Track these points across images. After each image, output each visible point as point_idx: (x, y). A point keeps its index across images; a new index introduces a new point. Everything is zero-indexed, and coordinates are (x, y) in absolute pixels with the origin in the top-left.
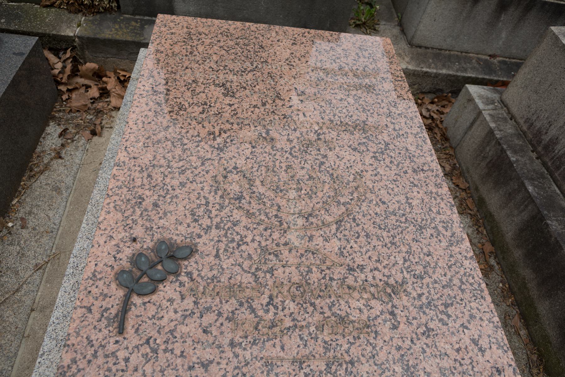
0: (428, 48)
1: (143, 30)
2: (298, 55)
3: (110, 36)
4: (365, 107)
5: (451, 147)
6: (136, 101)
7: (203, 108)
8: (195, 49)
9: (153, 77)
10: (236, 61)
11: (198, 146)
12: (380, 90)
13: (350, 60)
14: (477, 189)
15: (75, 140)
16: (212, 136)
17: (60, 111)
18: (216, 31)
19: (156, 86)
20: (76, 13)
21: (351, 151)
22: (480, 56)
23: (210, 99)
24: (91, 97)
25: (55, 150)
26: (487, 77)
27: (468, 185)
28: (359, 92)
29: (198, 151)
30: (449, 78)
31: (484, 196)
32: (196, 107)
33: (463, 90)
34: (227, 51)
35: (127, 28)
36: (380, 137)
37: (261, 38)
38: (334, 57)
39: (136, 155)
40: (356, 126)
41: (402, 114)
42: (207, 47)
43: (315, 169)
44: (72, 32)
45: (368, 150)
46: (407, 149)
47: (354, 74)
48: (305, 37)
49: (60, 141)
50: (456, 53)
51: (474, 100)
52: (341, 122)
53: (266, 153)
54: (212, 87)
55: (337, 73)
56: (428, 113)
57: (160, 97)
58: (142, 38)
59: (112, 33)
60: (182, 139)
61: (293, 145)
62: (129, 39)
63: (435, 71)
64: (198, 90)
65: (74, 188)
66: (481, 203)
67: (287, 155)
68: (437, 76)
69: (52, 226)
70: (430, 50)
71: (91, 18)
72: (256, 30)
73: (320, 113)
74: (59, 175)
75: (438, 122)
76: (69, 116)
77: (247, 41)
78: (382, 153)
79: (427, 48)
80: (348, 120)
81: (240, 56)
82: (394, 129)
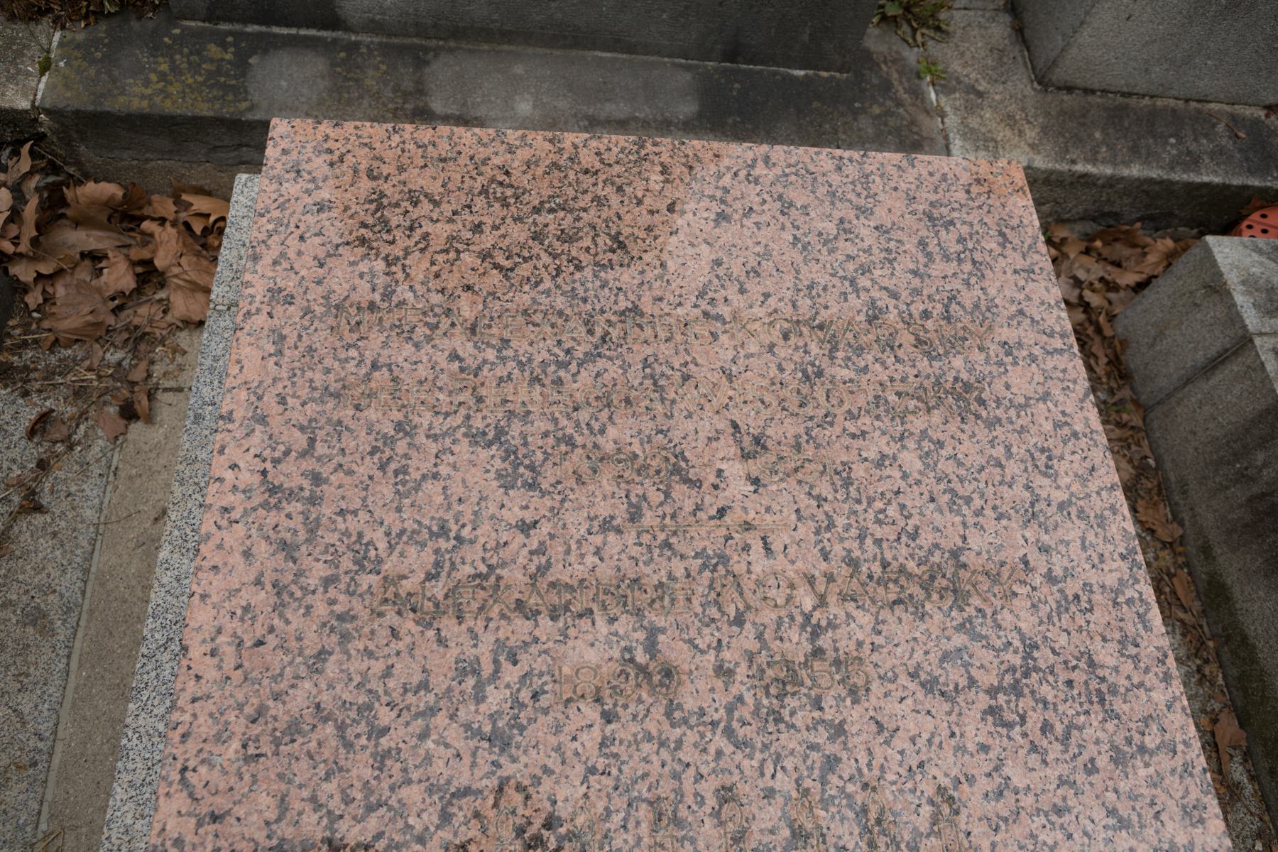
0: (1093, 92)
1: (244, 74)
2: (737, 270)
3: (145, 103)
4: (956, 485)
5: (1136, 403)
6: (212, 544)
7: (437, 551)
8: (400, 276)
9: (263, 420)
10: (537, 318)
11: (424, 736)
12: (998, 401)
13: (901, 279)
14: (1206, 550)
15: (79, 443)
16: (471, 681)
17: (24, 345)
18: (468, 182)
19: (276, 462)
20: (31, 19)
21: (920, 695)
22: (1240, 110)
23: (456, 507)
24: (111, 292)
25: (20, 483)
26: (1255, 182)
27: (1180, 532)
28: (936, 417)
29: (428, 759)
30: (1145, 187)
31: (1229, 582)
32: (412, 551)
33: (1196, 251)
34: (506, 272)
35: (195, 68)
36: (1006, 618)
37: (615, 200)
38: (851, 266)
39: (219, 800)
40: (932, 578)
41: (1070, 503)
42: (440, 258)
43: (807, 791)
44: (25, 95)
45: (972, 682)
46: (1092, 664)
47: (918, 339)
48: (756, 182)
49: (33, 451)
50: (1172, 102)
51: (1229, 293)
52: (885, 565)
53: (649, 738)
54: (463, 447)
55: (864, 339)
56: (1077, 292)
57: (289, 516)
58: (244, 105)
59: (149, 91)
60: (369, 707)
61: (734, 690)
62: (204, 110)
63: (1109, 171)
64: (419, 465)
65: (86, 607)
66: (1215, 595)
67: (720, 741)
68: (1111, 182)
69: (31, 743)
70: (1095, 99)
71: (80, 33)
72: (598, 165)
73: (817, 533)
74: (38, 570)
75: (1102, 319)
76: (53, 360)
77: (570, 218)
78: (1016, 690)
79: (1088, 91)
80: (904, 551)
81: (547, 293)
82: (1050, 578)
